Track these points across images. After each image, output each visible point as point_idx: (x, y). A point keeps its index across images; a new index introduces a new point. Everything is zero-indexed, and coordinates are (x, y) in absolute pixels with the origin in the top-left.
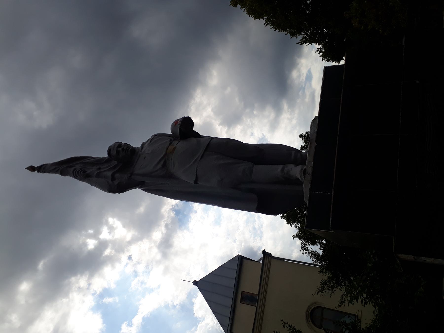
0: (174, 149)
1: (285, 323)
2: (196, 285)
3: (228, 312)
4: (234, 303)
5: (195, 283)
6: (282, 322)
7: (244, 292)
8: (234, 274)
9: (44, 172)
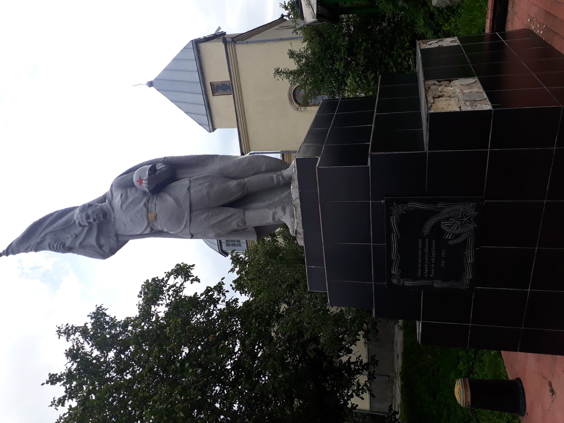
2: (152, 86)
3: (203, 110)
4: (206, 98)
5: (151, 84)
8: (194, 66)
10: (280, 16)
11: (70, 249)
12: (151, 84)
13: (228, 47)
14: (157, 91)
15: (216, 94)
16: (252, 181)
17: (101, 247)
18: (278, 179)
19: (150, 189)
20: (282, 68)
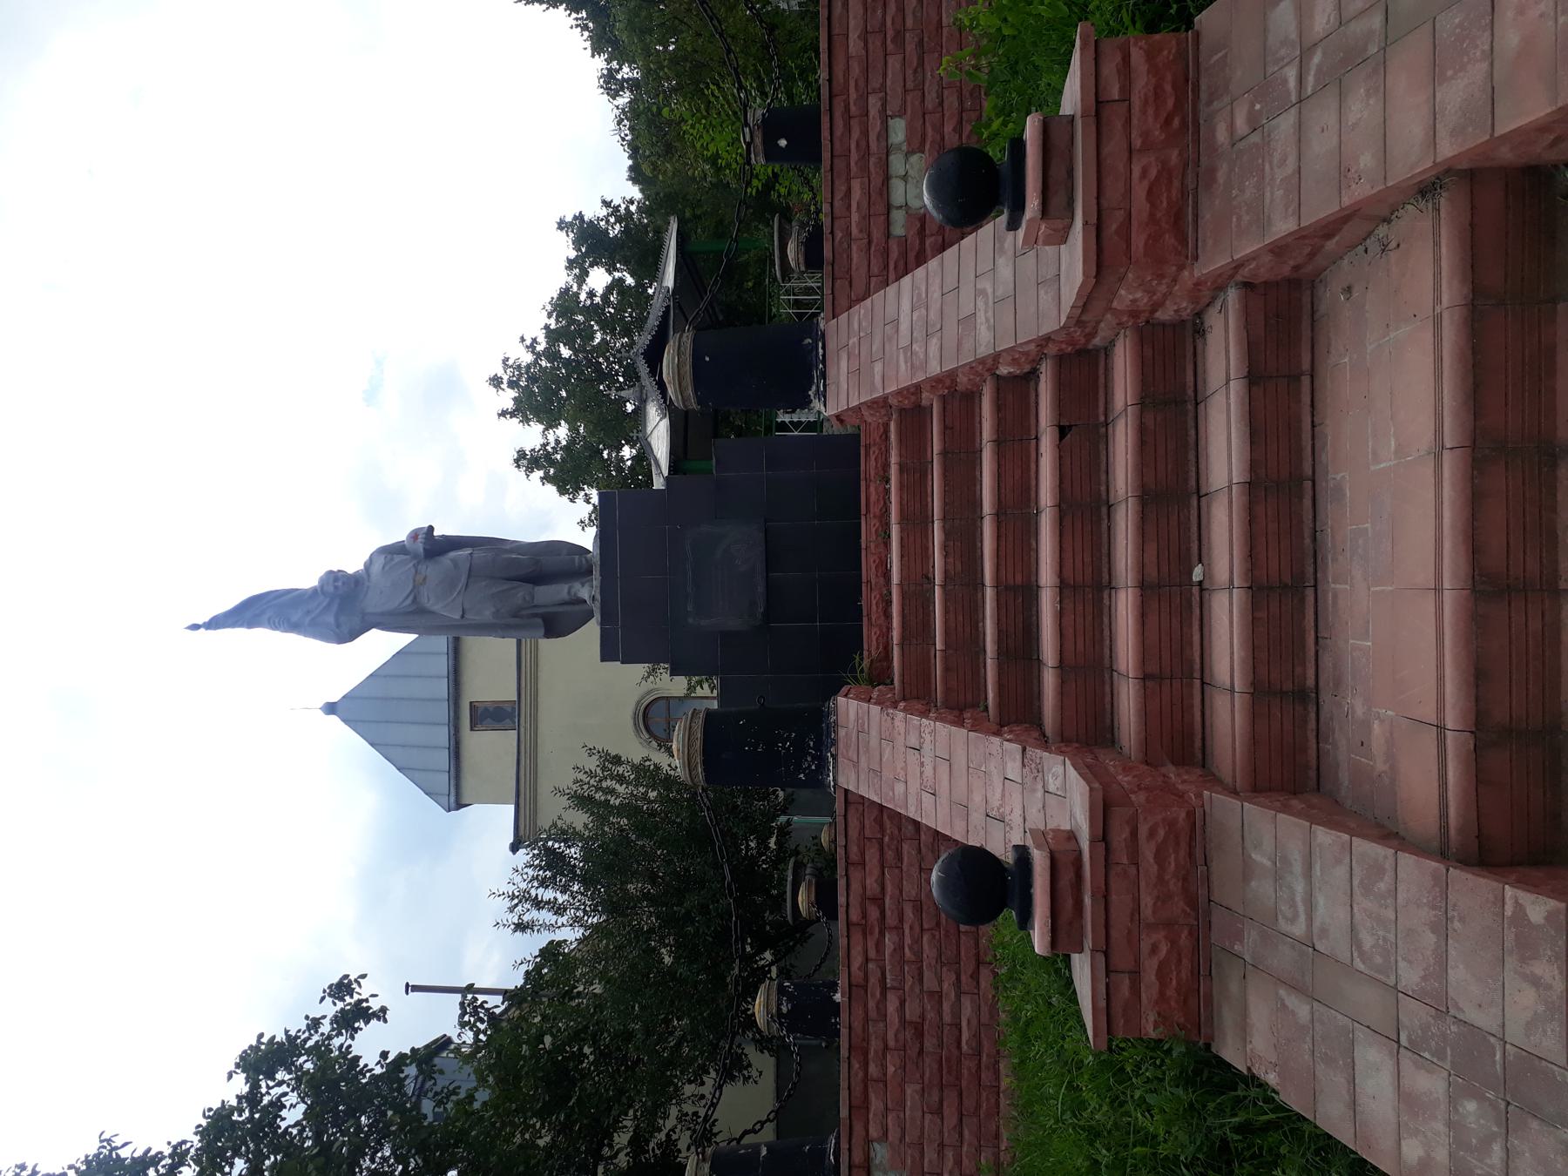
0: (425, 579)
1: (590, 749)
3: (443, 759)
5: (330, 708)
6: (586, 748)
7: (476, 704)
9: (219, 628)
12: (330, 708)
14: (343, 723)
17: (338, 626)
18: (581, 561)
19: (428, 547)
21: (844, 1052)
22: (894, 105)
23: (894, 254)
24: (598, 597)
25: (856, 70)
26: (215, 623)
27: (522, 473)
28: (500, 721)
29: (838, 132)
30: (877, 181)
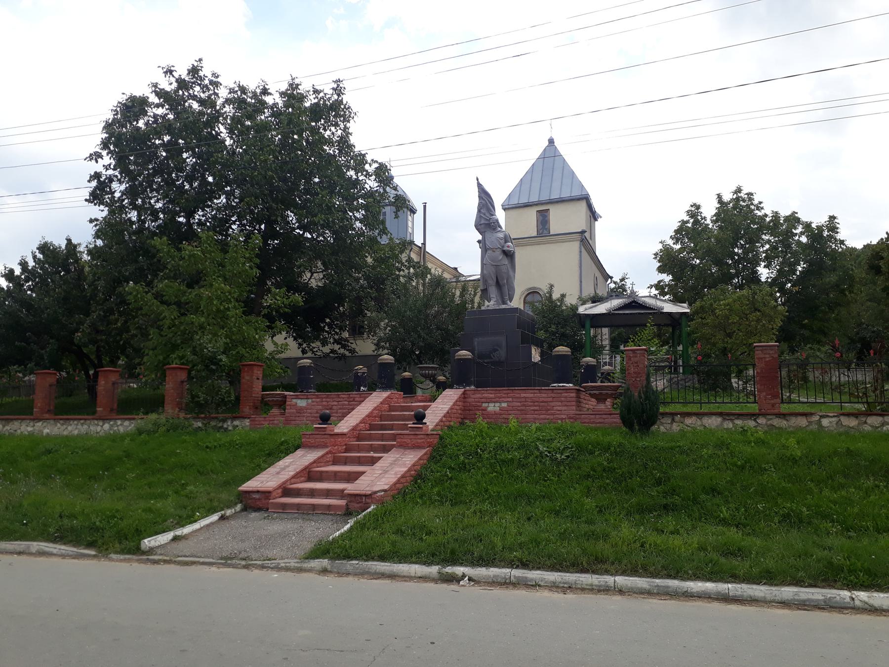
3: (524, 200)
5: (551, 141)
8: (566, 194)
10: (611, 275)
11: (479, 211)
12: (551, 141)
13: (578, 235)
15: (539, 214)
16: (506, 289)
17: (480, 225)
20: (554, 289)
21: (327, 393)
22: (510, 404)
23: (478, 404)
24: (489, 308)
25: (518, 395)
26: (479, 186)
27: (688, 208)
28: (541, 223)
29: (505, 392)
30: (493, 400)
